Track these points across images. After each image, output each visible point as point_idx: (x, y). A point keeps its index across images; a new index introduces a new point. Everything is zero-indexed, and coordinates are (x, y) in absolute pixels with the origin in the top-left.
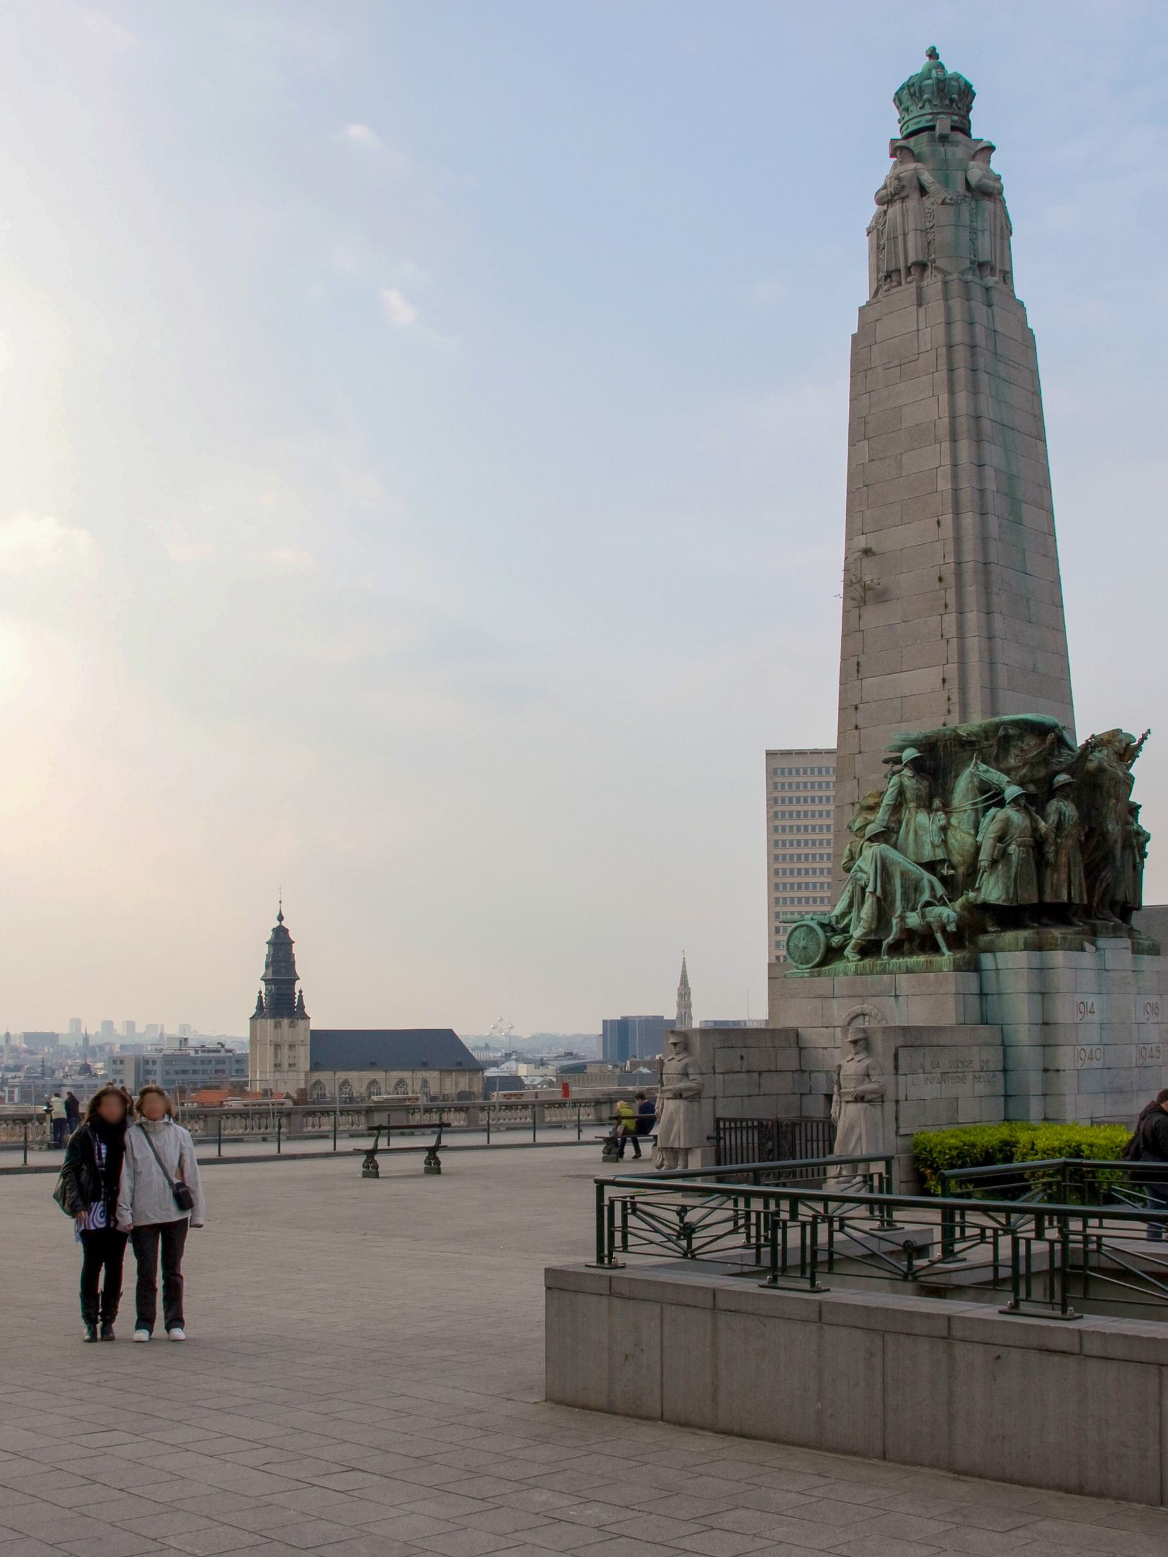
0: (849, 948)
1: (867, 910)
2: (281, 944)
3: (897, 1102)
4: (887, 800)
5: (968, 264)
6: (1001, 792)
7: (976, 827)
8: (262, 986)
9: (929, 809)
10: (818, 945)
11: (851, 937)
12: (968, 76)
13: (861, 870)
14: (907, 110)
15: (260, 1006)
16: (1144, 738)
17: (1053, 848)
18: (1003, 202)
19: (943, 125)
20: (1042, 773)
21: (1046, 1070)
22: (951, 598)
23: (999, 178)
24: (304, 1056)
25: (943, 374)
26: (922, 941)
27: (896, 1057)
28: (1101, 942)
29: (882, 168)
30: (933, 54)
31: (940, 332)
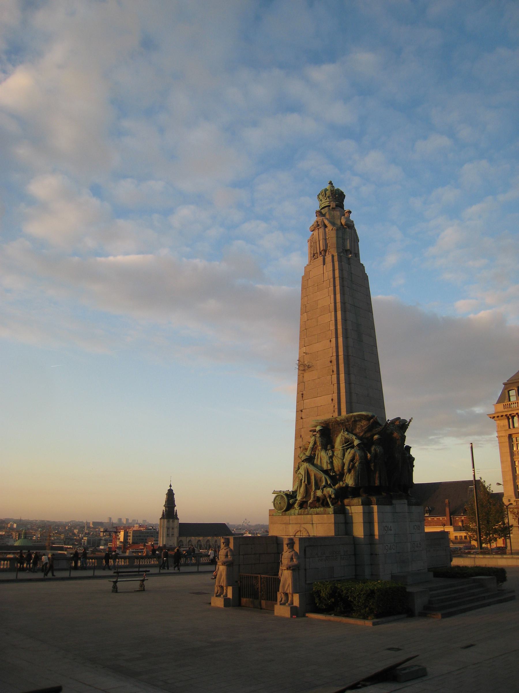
0: (296, 504)
1: (302, 489)
2: (170, 494)
3: (305, 570)
4: (311, 445)
5: (341, 250)
6: (353, 442)
7: (344, 455)
8: (164, 508)
9: (326, 450)
10: (285, 502)
11: (297, 500)
12: (342, 189)
13: (300, 473)
14: (321, 200)
15: (163, 515)
16: (410, 421)
17: (373, 464)
18: (355, 230)
19: (333, 205)
20: (368, 435)
21: (372, 554)
22: (335, 369)
23: (353, 221)
24: (176, 531)
25: (332, 288)
26: (322, 502)
27: (305, 550)
28: (394, 502)
29: (314, 219)
30: (331, 183)
31: (331, 273)
